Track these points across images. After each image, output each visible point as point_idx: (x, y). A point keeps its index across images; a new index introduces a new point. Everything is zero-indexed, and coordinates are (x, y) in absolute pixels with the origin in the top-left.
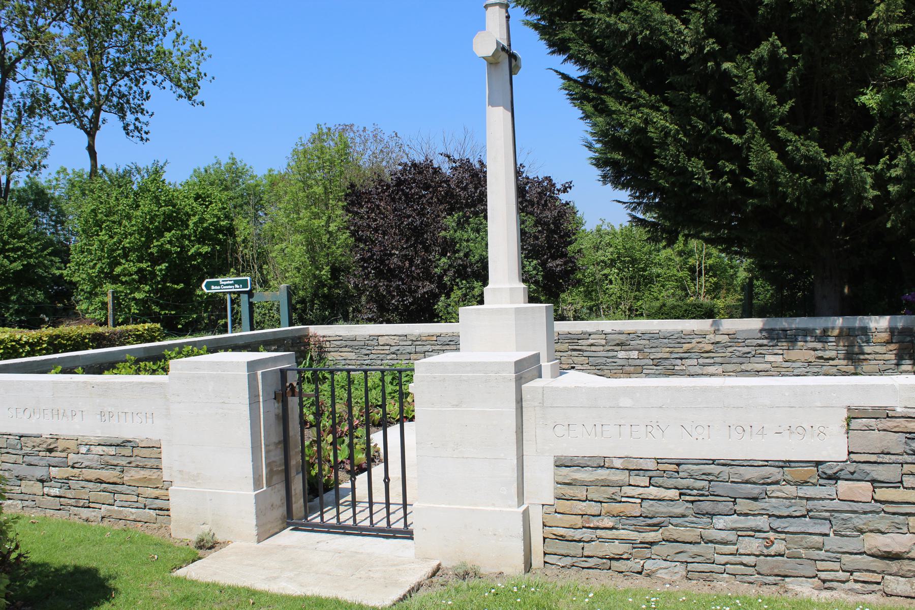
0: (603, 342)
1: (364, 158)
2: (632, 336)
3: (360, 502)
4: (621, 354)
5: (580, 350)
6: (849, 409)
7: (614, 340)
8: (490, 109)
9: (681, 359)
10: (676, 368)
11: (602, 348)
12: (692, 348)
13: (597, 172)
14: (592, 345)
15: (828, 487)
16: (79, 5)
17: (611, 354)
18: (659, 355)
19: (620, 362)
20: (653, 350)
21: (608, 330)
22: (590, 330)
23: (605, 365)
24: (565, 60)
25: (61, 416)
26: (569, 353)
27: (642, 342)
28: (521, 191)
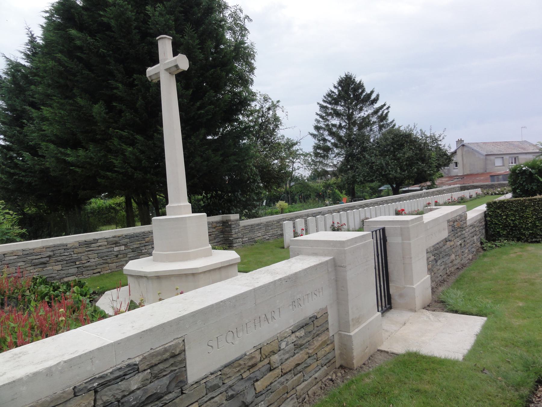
0: (106, 243)
2: (120, 238)
3: (365, 215)
4: (116, 249)
5: (92, 250)
6: (448, 221)
7: (112, 241)
9: (145, 246)
10: (143, 251)
13: (343, 76)
14: (100, 246)
15: (120, 362)
17: (110, 250)
18: (135, 246)
20: (132, 244)
21: (107, 236)
22: (96, 238)
24: (296, 144)
26: (86, 253)
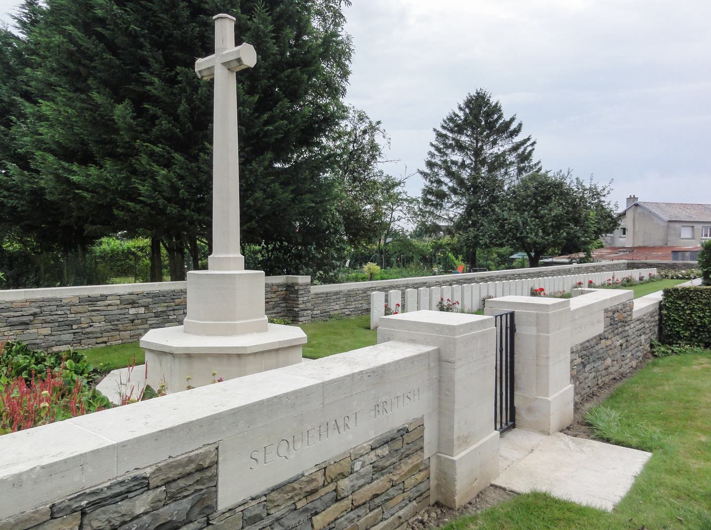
0: (118, 302)
1: (651, 309)
5: (98, 310)
7: (127, 300)
8: (661, 293)
9: (174, 310)
10: (171, 317)
11: (116, 307)
12: (182, 302)
16: (2, 214)
17: (123, 311)
19: (131, 318)
20: (155, 306)
22: (105, 293)
23: (118, 320)
25: (341, 430)
26: (88, 314)
27: (148, 300)
28: (531, 290)
